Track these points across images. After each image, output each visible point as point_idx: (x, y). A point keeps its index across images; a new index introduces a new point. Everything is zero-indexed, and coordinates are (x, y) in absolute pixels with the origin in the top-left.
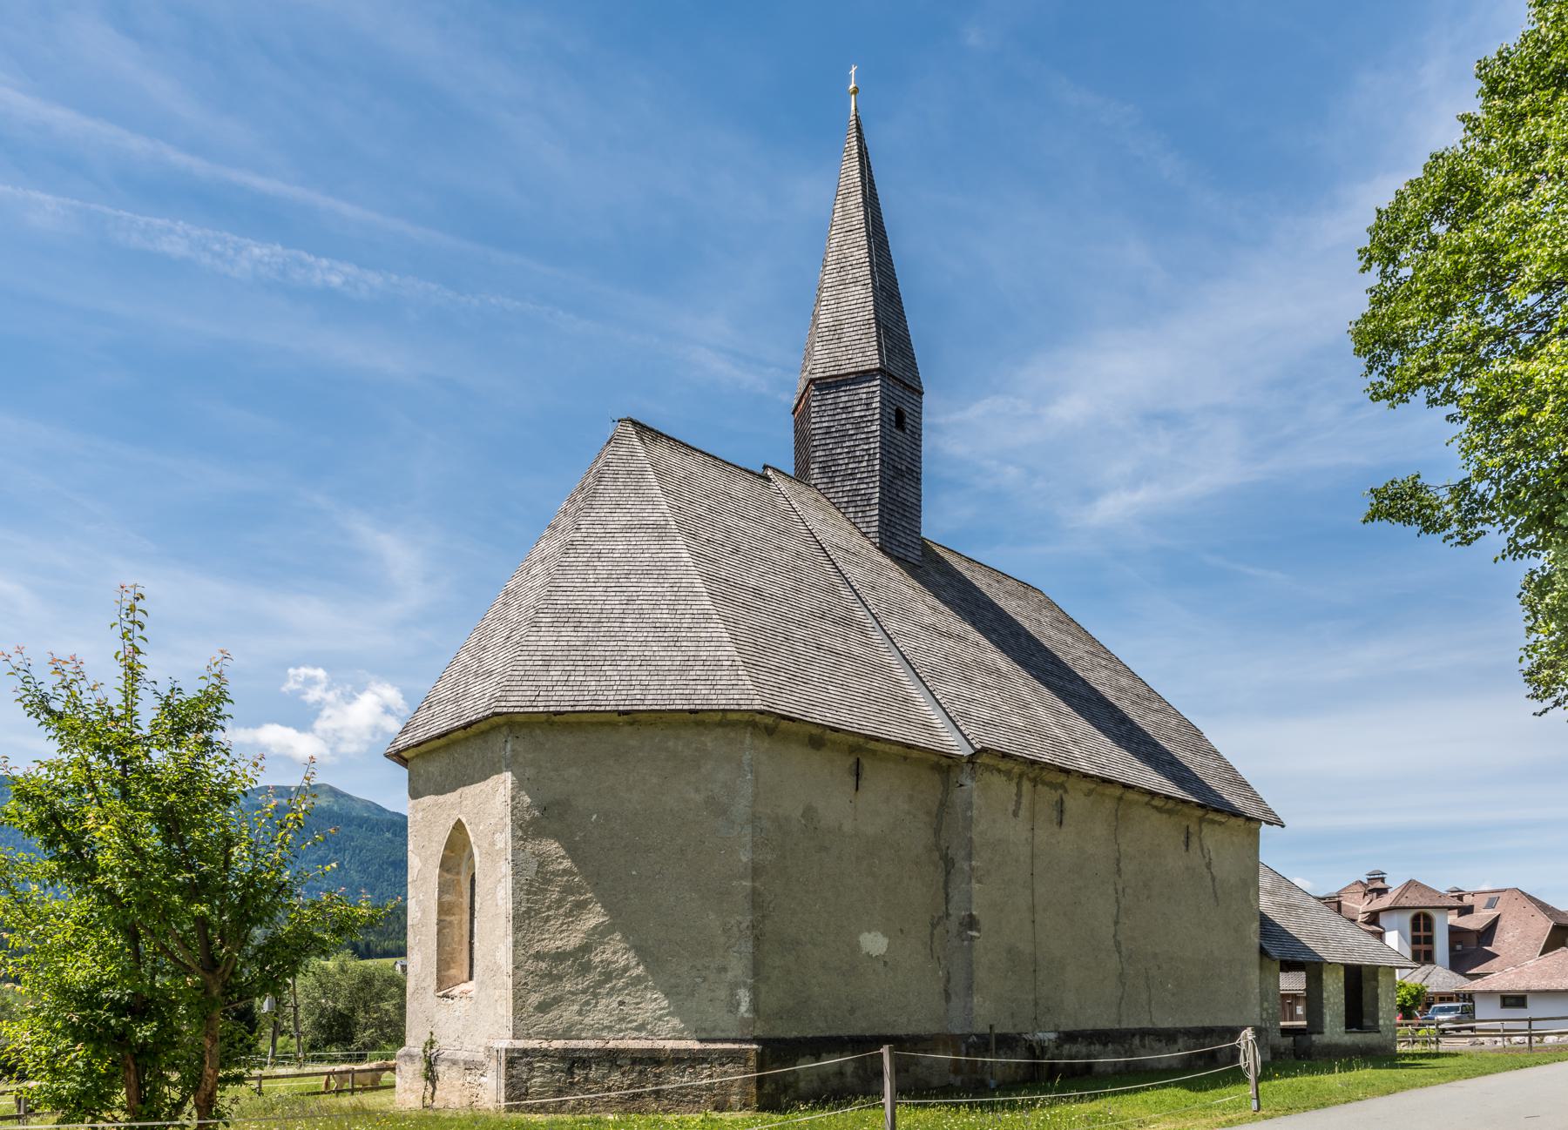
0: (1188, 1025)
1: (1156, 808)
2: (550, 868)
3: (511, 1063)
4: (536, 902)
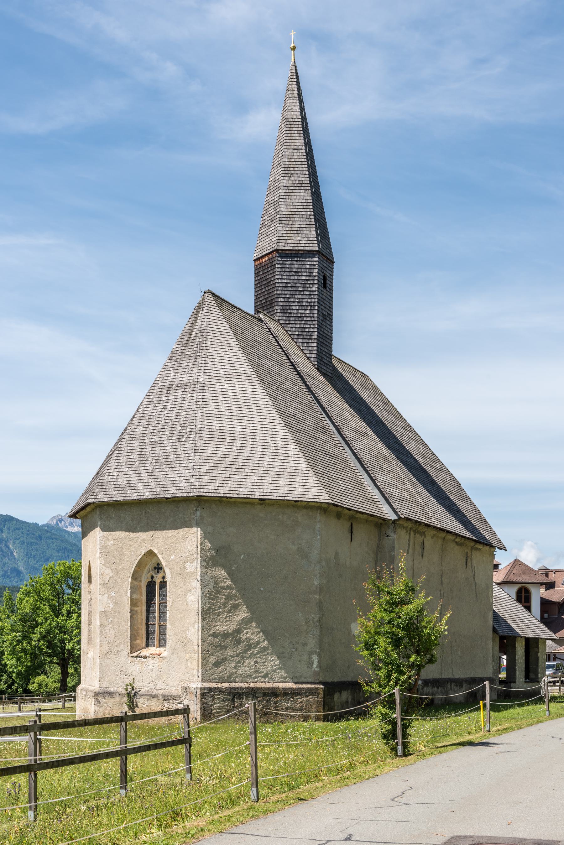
0: (466, 676)
1: (456, 543)
2: (220, 585)
3: (203, 695)
4: (213, 604)
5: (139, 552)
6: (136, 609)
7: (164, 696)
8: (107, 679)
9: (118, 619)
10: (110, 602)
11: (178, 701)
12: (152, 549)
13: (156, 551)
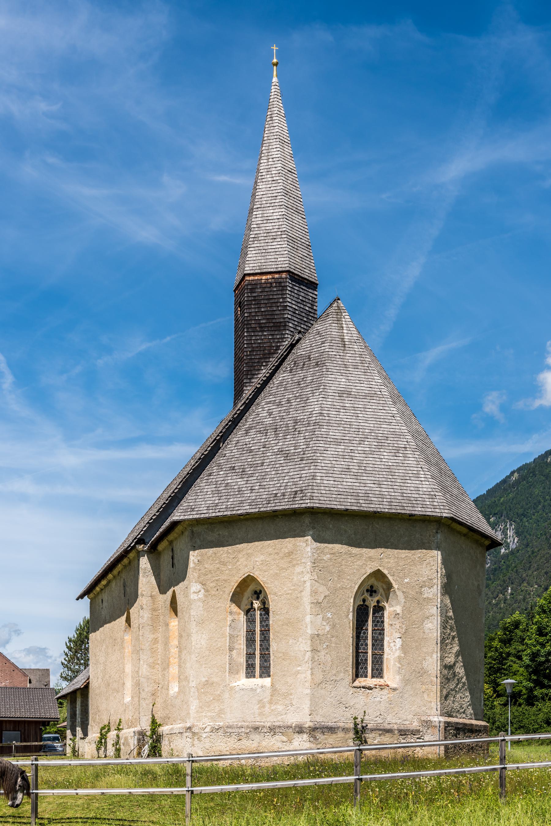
5: (363, 571)
7: (400, 731)
9: (336, 644)
10: (325, 624)
11: (417, 736)
12: (380, 568)
13: (385, 572)
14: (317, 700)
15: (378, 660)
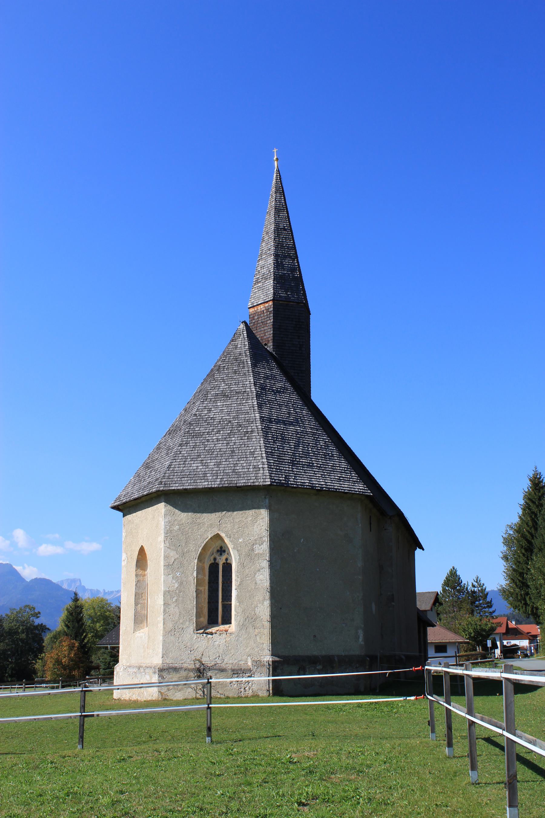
5: (206, 536)
6: (201, 588)
7: (233, 670)
8: (171, 655)
12: (219, 533)
13: (223, 535)
14: (168, 645)
15: (227, 609)
